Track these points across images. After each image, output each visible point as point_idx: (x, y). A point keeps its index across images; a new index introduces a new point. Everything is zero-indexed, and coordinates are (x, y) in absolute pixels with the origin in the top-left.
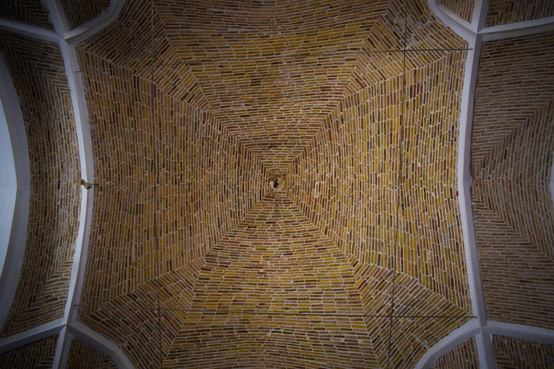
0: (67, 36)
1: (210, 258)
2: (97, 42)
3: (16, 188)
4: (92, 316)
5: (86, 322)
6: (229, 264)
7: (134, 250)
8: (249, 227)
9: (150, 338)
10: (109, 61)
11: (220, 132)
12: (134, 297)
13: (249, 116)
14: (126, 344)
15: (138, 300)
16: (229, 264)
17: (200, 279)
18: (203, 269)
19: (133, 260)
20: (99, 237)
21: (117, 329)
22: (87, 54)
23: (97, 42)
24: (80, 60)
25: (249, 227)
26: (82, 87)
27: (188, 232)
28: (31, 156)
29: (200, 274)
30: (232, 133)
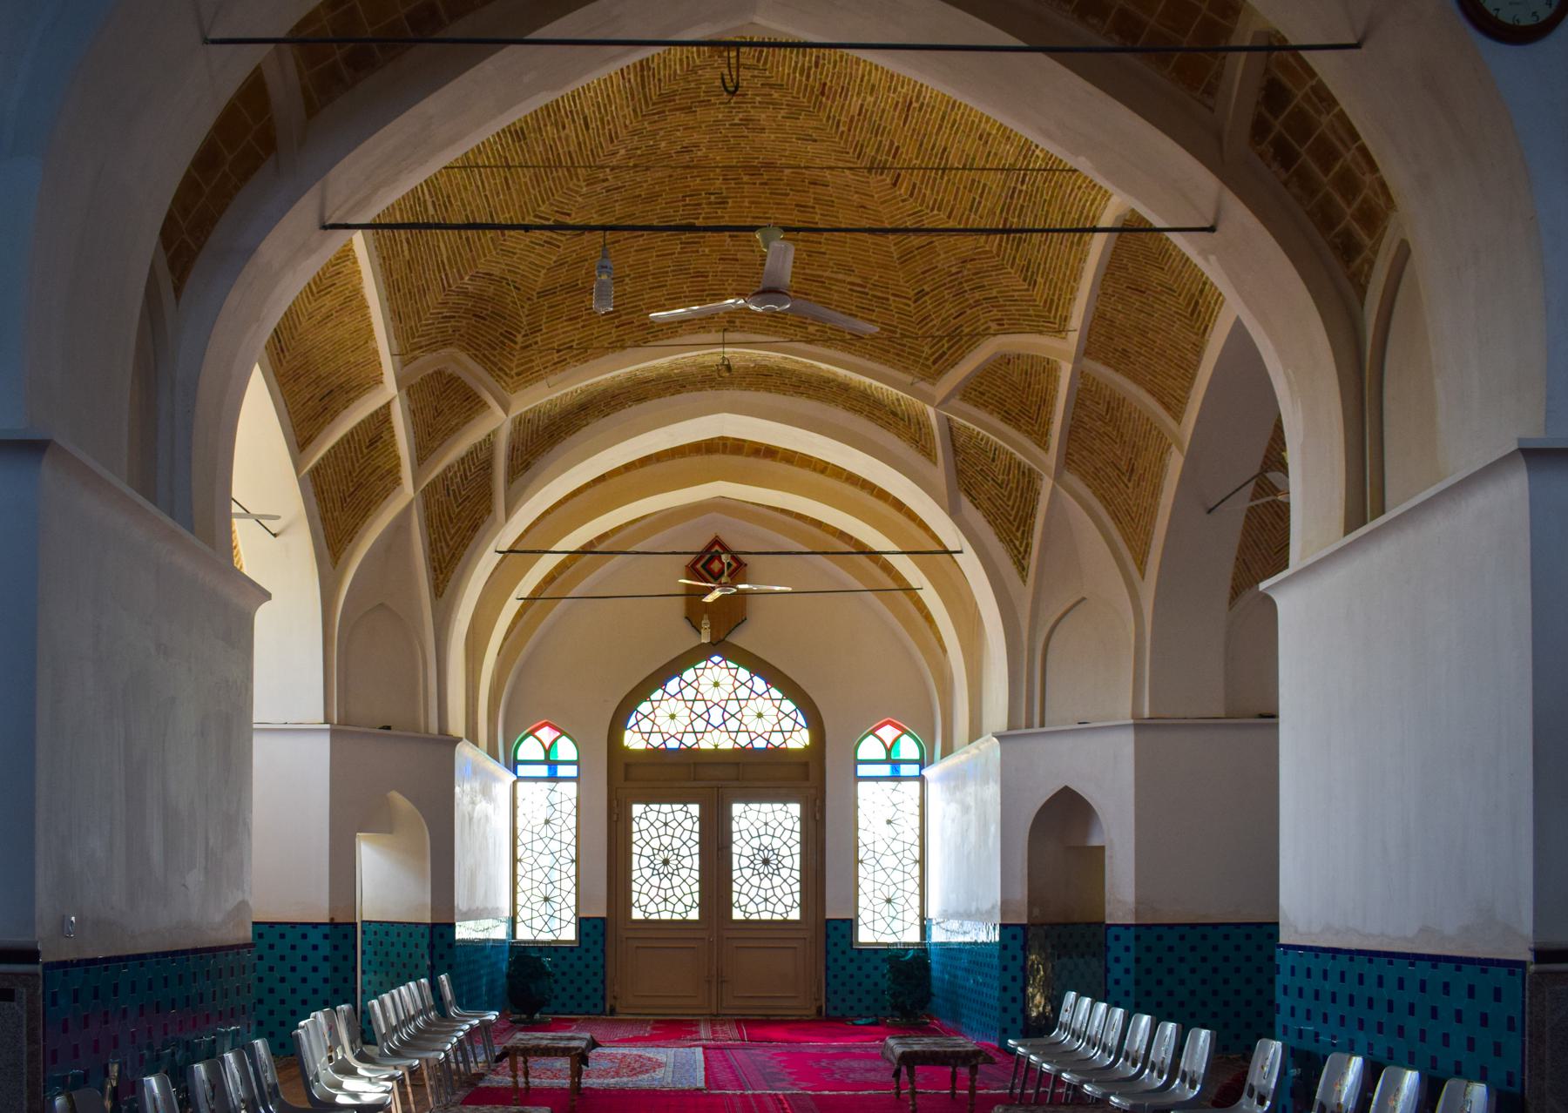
0: (499, 412)
1: (875, 168)
2: (495, 364)
3: (726, 415)
4: (934, 363)
5: (940, 373)
6: (892, 143)
7: (840, 276)
8: (823, 94)
9: (994, 292)
10: (519, 338)
11: (622, 152)
12: (921, 294)
13: (585, 119)
14: (994, 326)
15: (926, 288)
16: (892, 143)
17: (911, 195)
18: (895, 185)
19: (859, 281)
20: (812, 329)
21: (967, 330)
22: (518, 374)
23: (495, 364)
24: (529, 382)
25: (823, 94)
26: (569, 371)
27: (819, 189)
28: (679, 392)
29: (903, 190)
30: (623, 133)
